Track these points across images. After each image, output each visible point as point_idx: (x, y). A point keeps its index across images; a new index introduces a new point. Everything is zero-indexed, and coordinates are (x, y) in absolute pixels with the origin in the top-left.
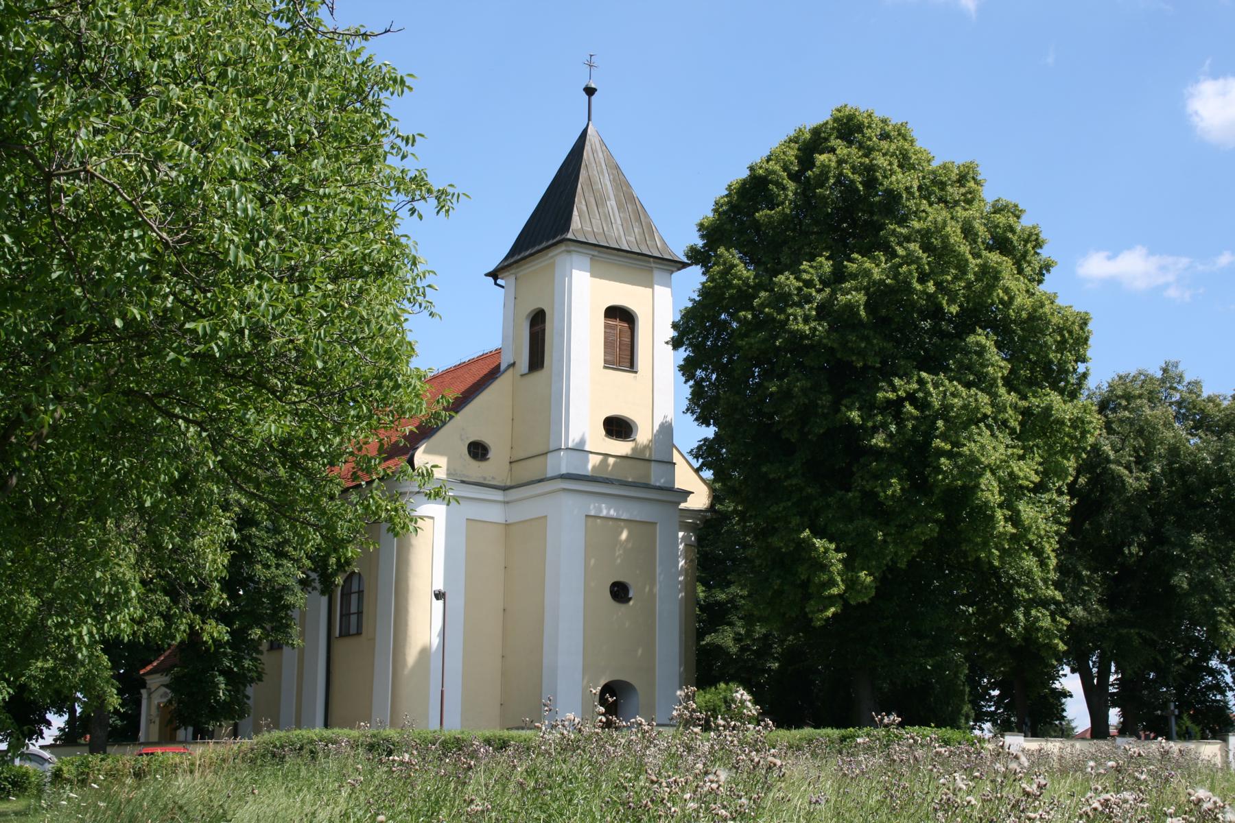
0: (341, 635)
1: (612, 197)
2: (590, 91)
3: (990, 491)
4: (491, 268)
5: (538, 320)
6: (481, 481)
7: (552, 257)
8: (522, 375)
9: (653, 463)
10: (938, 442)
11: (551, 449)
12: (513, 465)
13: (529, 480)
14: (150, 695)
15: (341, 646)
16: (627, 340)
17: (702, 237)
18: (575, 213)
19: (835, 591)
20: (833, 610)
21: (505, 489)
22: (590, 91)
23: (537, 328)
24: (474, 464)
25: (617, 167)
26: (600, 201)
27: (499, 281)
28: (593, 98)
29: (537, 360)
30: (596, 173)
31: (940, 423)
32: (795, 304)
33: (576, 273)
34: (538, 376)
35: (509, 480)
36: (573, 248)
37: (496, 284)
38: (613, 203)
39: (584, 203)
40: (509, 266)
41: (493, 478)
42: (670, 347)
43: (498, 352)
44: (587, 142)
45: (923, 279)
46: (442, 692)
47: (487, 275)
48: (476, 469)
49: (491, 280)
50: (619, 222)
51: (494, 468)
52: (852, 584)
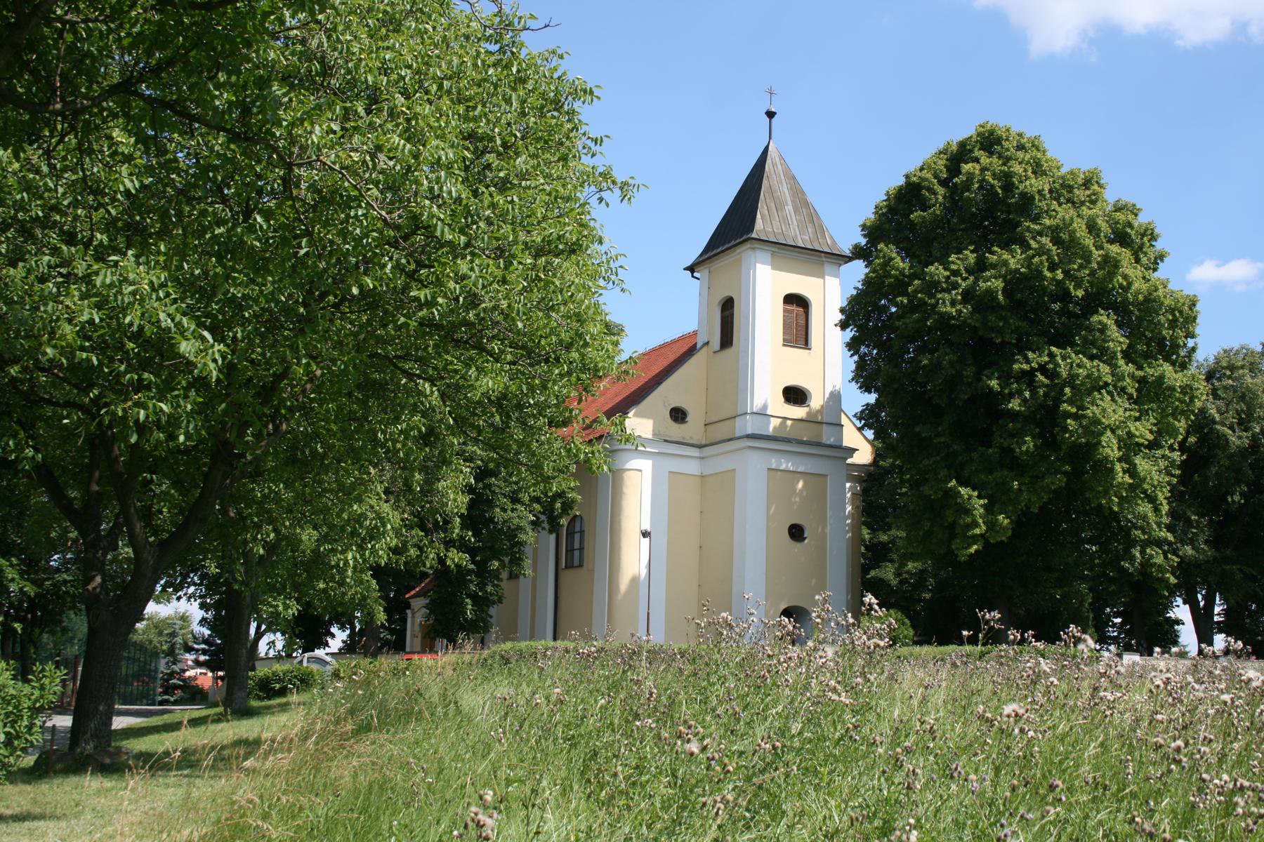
1: (789, 202)
2: (771, 115)
3: (1110, 448)
4: (689, 264)
5: (728, 306)
6: (681, 440)
9: (824, 426)
10: (1065, 406)
14: (413, 614)
15: (567, 576)
16: (802, 322)
17: (865, 236)
18: (759, 216)
19: (977, 531)
20: (975, 547)
21: (700, 447)
22: (771, 115)
23: (727, 313)
25: (794, 178)
26: (779, 207)
27: (695, 274)
29: (727, 339)
31: (1067, 390)
32: (943, 290)
33: (760, 267)
34: (728, 352)
36: (756, 246)
40: (703, 261)
42: (839, 328)
43: (695, 333)
44: (768, 157)
45: (1052, 268)
47: (685, 269)
48: (676, 430)
49: (689, 273)
50: (795, 223)
51: (693, 429)
52: (991, 525)
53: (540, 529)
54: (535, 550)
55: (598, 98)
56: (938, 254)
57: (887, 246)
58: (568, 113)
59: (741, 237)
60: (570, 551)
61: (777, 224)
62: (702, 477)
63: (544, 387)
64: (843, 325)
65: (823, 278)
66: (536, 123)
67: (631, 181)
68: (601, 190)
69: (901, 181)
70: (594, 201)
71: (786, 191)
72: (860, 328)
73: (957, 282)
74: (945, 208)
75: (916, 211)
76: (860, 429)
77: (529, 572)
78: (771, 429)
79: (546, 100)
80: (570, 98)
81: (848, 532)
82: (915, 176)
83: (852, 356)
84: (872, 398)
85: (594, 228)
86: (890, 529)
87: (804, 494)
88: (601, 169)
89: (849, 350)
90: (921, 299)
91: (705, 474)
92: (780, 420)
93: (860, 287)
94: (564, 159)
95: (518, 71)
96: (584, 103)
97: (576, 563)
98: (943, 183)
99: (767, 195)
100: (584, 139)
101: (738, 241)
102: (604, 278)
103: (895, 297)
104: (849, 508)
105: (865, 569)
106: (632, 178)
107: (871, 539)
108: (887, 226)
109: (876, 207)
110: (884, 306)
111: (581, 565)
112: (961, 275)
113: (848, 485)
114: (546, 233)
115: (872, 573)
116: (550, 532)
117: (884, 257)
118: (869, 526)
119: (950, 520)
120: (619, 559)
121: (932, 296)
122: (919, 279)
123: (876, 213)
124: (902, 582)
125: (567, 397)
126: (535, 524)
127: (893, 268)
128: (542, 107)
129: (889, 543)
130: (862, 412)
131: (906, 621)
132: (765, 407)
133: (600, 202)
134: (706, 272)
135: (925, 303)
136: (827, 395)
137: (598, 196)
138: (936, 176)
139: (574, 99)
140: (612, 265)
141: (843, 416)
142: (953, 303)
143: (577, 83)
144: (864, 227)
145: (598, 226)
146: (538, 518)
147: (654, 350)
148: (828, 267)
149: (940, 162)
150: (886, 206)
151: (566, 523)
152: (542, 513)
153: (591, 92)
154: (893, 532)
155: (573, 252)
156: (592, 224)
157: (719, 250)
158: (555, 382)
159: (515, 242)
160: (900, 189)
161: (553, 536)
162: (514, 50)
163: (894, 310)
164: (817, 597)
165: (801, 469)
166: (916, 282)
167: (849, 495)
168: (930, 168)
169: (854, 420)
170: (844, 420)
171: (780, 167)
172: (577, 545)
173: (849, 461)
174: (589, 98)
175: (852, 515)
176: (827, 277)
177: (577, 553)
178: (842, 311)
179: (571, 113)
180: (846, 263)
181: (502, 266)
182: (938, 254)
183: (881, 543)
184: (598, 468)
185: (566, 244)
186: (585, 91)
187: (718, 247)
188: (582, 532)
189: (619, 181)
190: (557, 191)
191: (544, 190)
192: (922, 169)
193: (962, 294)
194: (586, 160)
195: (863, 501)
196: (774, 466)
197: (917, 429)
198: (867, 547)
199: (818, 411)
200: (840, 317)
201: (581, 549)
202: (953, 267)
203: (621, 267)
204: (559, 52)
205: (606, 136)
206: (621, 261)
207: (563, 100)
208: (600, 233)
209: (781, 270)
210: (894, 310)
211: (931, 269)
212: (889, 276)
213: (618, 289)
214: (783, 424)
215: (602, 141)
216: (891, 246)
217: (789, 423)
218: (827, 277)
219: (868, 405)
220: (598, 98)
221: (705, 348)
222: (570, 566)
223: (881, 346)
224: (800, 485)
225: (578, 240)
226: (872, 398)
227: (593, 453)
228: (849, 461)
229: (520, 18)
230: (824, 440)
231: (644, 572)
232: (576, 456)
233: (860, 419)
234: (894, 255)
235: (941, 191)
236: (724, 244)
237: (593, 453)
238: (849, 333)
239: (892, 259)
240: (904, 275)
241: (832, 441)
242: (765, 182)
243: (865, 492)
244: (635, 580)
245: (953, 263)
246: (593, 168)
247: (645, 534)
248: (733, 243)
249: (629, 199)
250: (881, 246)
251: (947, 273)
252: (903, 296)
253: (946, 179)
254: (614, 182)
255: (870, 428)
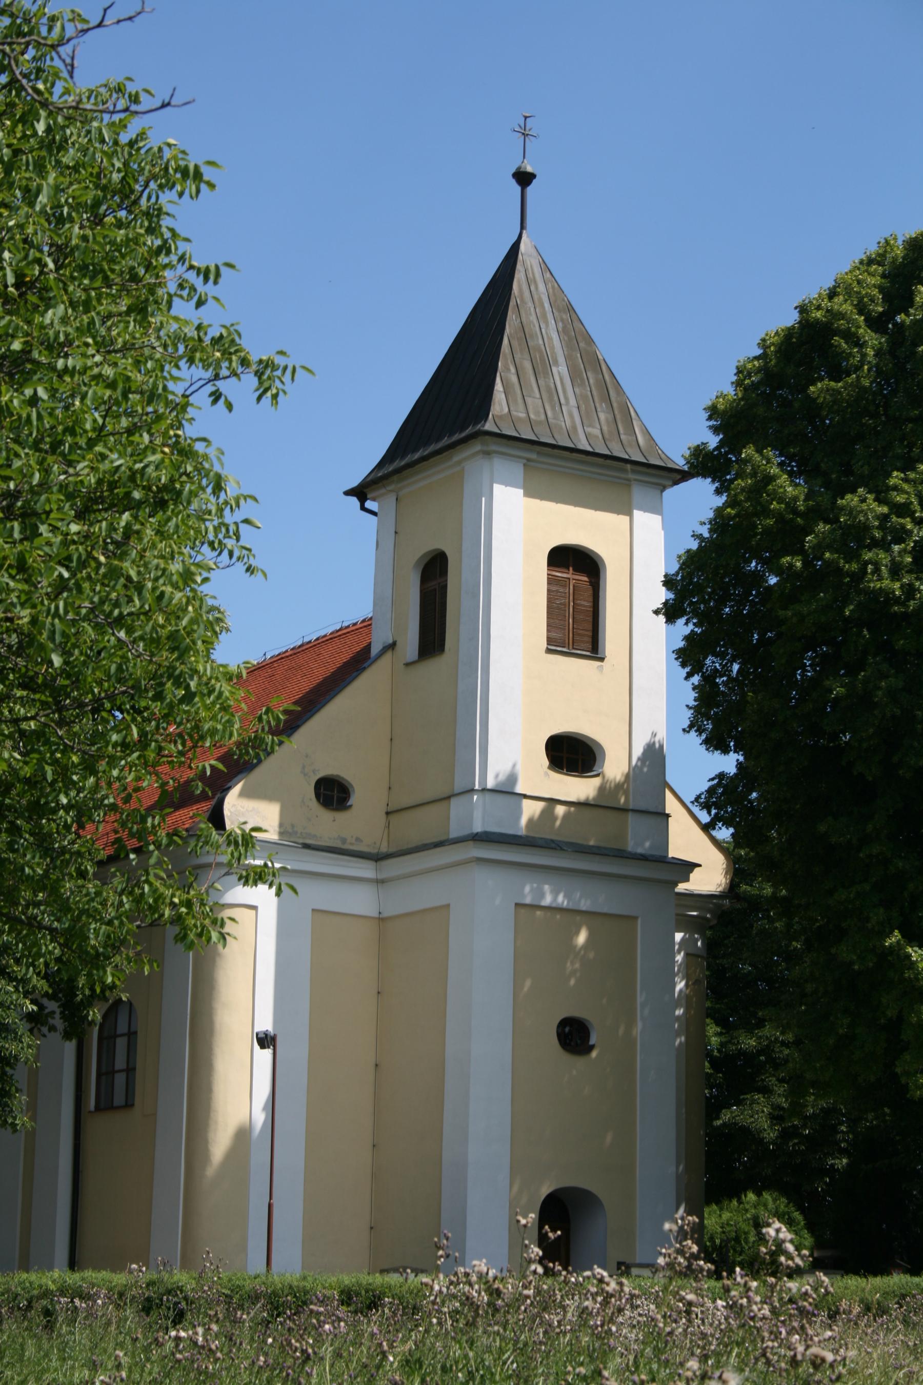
0: (98, 1108)
1: (561, 359)
2: (524, 179)
4: (354, 482)
6: (338, 844)
7: (459, 462)
8: (407, 665)
9: (631, 817)
11: (457, 790)
12: (391, 817)
13: (412, 845)
16: (586, 604)
17: (716, 430)
18: (499, 386)
21: (377, 858)
22: (524, 179)
24: (326, 815)
25: (570, 309)
26: (542, 367)
28: (529, 189)
30: (533, 318)
32: (875, 544)
33: (499, 490)
34: (436, 666)
35: (385, 844)
36: (494, 448)
37: (363, 508)
38: (563, 369)
39: (513, 370)
41: (358, 840)
42: (662, 618)
43: (367, 624)
44: (519, 267)
46: (270, 1206)
47: (348, 493)
49: (354, 501)
50: (573, 402)
53: (45, 1030)
54: (34, 1074)
55: (211, 186)
56: (866, 470)
57: (759, 451)
58: (147, 214)
59: (462, 429)
60: (106, 1073)
61: (534, 402)
62: (381, 920)
63: (89, 767)
64: (671, 612)
65: (630, 514)
66: (84, 238)
67: (279, 360)
68: (217, 377)
69: (791, 318)
70: (201, 398)
71: (555, 336)
72: (703, 618)
73: (903, 527)
74: (879, 372)
75: (821, 379)
76: (707, 828)
77: (22, 1120)
78: (524, 821)
79: (104, 189)
80: (153, 185)
81: (678, 1034)
82: (819, 308)
83: (689, 676)
84: (729, 763)
85: (206, 457)
86: (761, 1024)
87: (591, 955)
88: (214, 332)
89: (683, 665)
90: (827, 563)
91: (385, 914)
92: (541, 805)
93: (706, 535)
94: (140, 310)
95: (49, 130)
96: (181, 195)
97: (119, 1099)
98: (877, 323)
99: (515, 344)
100: (181, 269)
101: (456, 437)
102: (211, 544)
103: (778, 555)
104: (680, 985)
105: (713, 1108)
106: (281, 353)
107: (722, 1044)
108: (761, 411)
109: (739, 371)
110: (755, 573)
111: (129, 1104)
112: (911, 514)
113: (679, 936)
114: (105, 466)
115: (726, 1116)
116: (67, 1036)
117: (754, 474)
118: (721, 1021)
119: (891, 1013)
120: (209, 1090)
121: (853, 555)
122: (826, 521)
123: (738, 384)
124: (786, 1135)
125: (137, 790)
126: (35, 1020)
127: (774, 496)
128: (97, 203)
129: (760, 1052)
130: (711, 791)
131: (797, 1215)
132: (512, 778)
133: (215, 401)
134: (391, 500)
135: (839, 570)
136: (638, 751)
137: (210, 388)
138: (861, 309)
139: (161, 187)
140: (229, 518)
141: (668, 794)
142: (896, 571)
143: (167, 154)
144: (713, 412)
145: (212, 452)
146: (41, 1007)
147: (281, 658)
148: (638, 493)
149: (871, 280)
150: (759, 370)
151: (99, 1017)
152: (53, 997)
153: (198, 175)
154: (768, 1031)
155: (161, 504)
156: (199, 447)
157: (417, 456)
158: (112, 761)
159: (44, 485)
160: (789, 333)
161: (70, 1047)
162: (41, 86)
163: (773, 580)
164: (667, 1226)
165: (584, 905)
166: (822, 527)
167: (679, 958)
168: (849, 291)
169: (696, 810)
170: (671, 805)
171: (542, 287)
172: (120, 1062)
173: (682, 887)
174: (191, 186)
175: (686, 1000)
176: (637, 514)
177: (120, 1080)
178: (669, 582)
179: (154, 215)
180: (676, 483)
181: (17, 535)
182: (866, 470)
183: (742, 1053)
184: (200, 935)
185: (148, 488)
186: (185, 172)
187: (415, 450)
188: (132, 1035)
189: (254, 358)
190: (128, 379)
191: (100, 375)
192: (832, 294)
193: (914, 552)
194: (183, 309)
195: (709, 967)
196: (528, 901)
197: (822, 828)
198: (714, 1063)
199: (619, 786)
200: (661, 595)
201: (130, 1070)
202: (900, 499)
203: (247, 521)
204: (131, 88)
205: (229, 265)
206: (247, 510)
207: (138, 188)
208: (217, 468)
209: (542, 498)
210: (773, 580)
211: (850, 500)
212: (765, 512)
213: (240, 567)
214: (548, 814)
215: (218, 275)
216: (769, 452)
217: (560, 810)
218: (637, 514)
219: (721, 776)
220: (211, 186)
221: (388, 657)
222: (105, 1105)
223: (746, 655)
224: (582, 938)
225: (172, 480)
226: (729, 763)
227: (189, 904)
228: (682, 887)
229: (53, 19)
230: (631, 846)
231: (260, 1118)
232: (153, 909)
233: (707, 806)
234: (774, 470)
235: (872, 340)
236: (426, 444)
237: (189, 904)
238: (683, 628)
239: (770, 479)
240: (795, 511)
241: (646, 847)
242: (511, 316)
243: (710, 945)
244: (243, 1135)
245: (895, 488)
246: (199, 328)
247: (265, 1041)
248: (445, 441)
249: (275, 397)
250: (748, 452)
251: (885, 510)
252: (793, 554)
253: (881, 314)
254: (244, 362)
255: (727, 824)
